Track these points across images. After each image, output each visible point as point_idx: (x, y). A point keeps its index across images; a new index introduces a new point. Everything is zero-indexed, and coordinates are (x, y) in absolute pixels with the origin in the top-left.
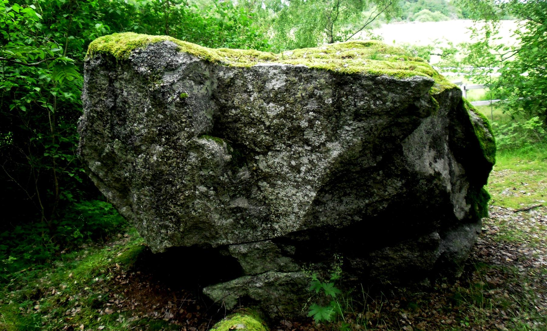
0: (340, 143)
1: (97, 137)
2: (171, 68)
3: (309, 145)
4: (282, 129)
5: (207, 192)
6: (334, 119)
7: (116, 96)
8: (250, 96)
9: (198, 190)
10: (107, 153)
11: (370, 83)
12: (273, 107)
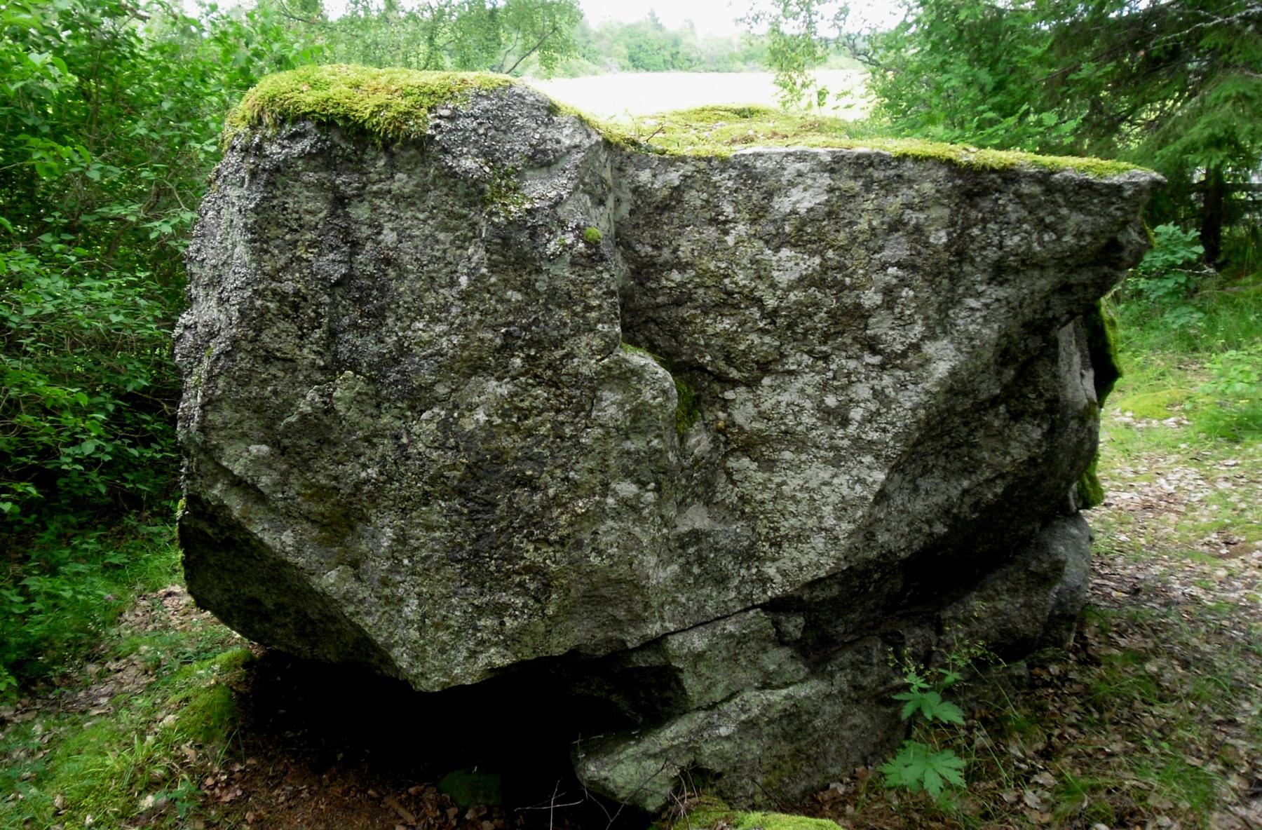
0: (952, 341)
1: (273, 371)
2: (542, 160)
3: (874, 351)
4: (810, 316)
5: (638, 497)
6: (945, 282)
7: (356, 246)
8: (726, 233)
9: (615, 494)
10: (304, 417)
11: (1036, 189)
12: (789, 259)
